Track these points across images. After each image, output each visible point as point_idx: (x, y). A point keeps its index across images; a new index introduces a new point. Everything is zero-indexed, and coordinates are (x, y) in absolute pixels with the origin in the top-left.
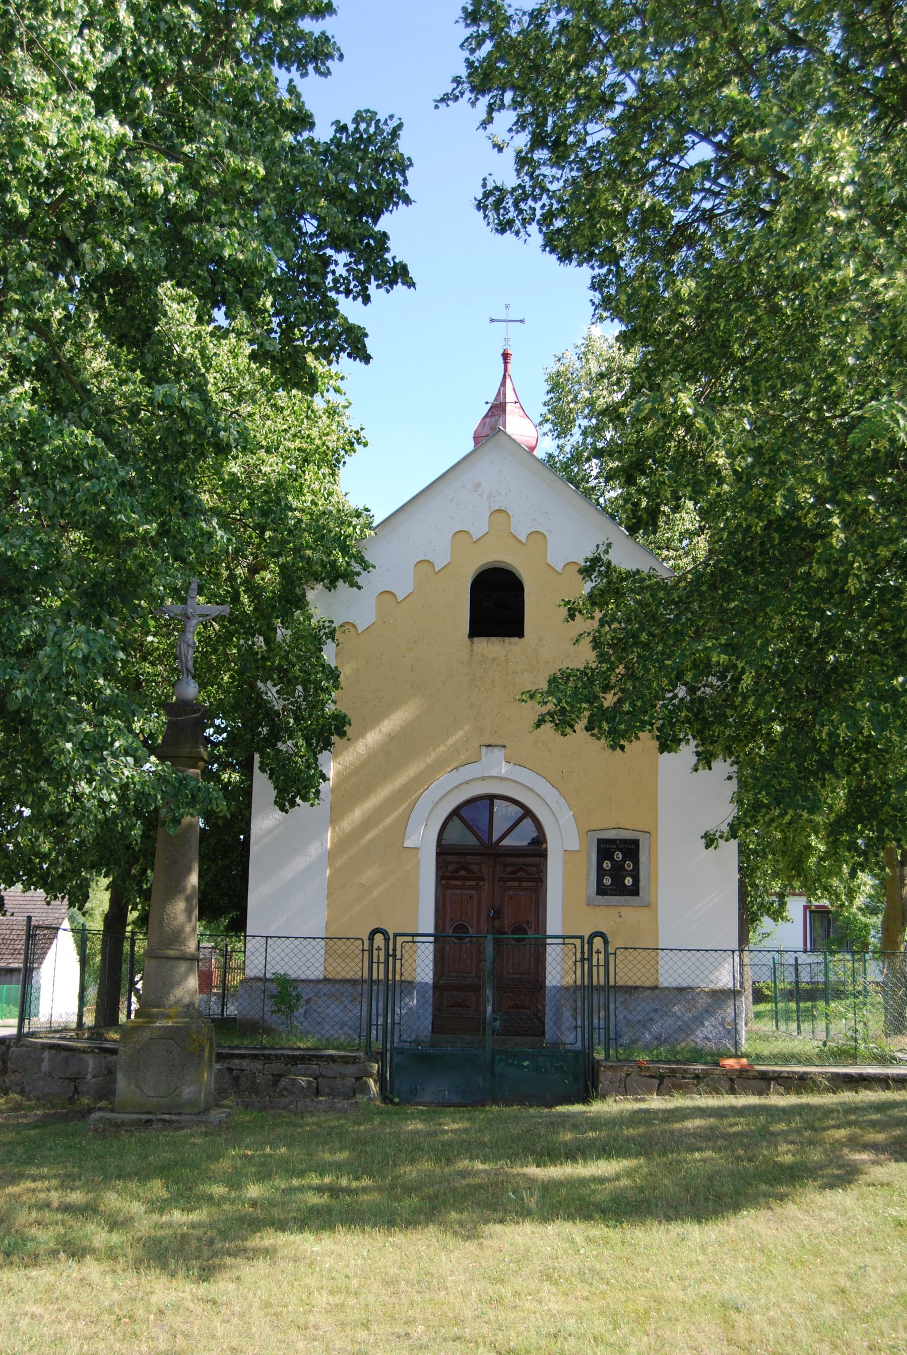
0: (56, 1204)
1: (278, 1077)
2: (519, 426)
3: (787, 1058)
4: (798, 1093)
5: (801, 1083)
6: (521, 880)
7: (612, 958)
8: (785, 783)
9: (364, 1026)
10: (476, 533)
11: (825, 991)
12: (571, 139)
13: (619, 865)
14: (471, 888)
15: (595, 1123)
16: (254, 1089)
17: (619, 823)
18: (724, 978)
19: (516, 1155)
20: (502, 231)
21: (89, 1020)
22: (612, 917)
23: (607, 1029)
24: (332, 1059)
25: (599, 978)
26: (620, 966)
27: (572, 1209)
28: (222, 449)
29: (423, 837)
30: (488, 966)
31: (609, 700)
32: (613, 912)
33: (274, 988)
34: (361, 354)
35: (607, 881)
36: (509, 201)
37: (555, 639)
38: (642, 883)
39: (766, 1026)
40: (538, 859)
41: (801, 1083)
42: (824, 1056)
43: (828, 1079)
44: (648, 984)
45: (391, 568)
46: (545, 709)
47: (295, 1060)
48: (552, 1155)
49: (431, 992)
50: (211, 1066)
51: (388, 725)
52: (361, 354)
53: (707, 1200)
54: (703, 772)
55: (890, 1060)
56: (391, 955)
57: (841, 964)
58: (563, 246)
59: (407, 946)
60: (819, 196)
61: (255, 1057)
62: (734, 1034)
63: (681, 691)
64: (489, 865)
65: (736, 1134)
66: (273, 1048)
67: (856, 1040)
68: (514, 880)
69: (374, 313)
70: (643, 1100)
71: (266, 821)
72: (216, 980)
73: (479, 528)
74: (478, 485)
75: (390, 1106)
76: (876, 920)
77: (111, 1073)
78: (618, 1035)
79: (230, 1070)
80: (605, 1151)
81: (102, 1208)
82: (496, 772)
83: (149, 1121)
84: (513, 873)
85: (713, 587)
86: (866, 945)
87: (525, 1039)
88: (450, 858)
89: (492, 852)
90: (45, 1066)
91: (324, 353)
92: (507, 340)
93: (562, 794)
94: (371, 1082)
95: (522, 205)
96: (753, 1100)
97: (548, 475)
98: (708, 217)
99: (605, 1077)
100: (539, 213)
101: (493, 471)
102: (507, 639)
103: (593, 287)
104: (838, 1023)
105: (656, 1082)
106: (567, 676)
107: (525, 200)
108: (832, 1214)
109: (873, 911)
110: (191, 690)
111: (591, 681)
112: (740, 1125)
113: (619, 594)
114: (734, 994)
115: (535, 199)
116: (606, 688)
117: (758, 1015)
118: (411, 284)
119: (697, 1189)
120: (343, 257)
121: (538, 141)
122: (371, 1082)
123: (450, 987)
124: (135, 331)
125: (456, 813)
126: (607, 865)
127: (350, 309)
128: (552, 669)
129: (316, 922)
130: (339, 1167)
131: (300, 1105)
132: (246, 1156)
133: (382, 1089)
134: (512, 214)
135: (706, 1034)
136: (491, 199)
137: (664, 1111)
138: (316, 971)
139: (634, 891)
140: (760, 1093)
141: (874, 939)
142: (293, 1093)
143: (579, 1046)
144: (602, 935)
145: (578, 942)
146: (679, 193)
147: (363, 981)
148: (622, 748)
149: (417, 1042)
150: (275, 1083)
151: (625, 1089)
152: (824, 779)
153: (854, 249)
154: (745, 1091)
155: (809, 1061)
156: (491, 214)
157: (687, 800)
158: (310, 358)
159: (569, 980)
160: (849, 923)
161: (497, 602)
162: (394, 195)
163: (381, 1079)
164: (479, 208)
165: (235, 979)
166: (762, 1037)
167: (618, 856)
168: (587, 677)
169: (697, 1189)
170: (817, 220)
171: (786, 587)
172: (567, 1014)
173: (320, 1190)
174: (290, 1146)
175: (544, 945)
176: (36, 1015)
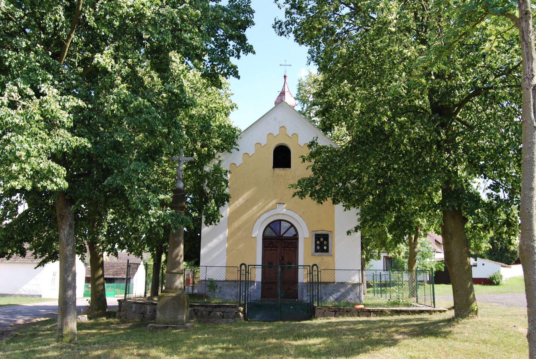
0: (135, 354)
1: (210, 312)
2: (289, 100)
3: (376, 305)
4: (380, 316)
5: (381, 313)
6: (290, 247)
7: (319, 273)
8: (375, 213)
9: (239, 294)
10: (275, 135)
11: (390, 284)
12: (304, 6)
13: (322, 242)
14: (274, 250)
15: (313, 326)
16: (202, 316)
17: (322, 229)
18: (356, 279)
19: (288, 337)
20: (281, 35)
21: (149, 295)
22: (320, 259)
23: (318, 296)
24: (228, 306)
25: (315, 280)
26: (322, 275)
27: (305, 354)
28: (187, 106)
29: (258, 233)
30: (279, 275)
31: (318, 188)
32: (320, 258)
33: (209, 283)
34: (236, 75)
35: (318, 248)
36: (283, 26)
37: (300, 169)
38: (330, 248)
39: (371, 295)
40: (294, 241)
41: (381, 313)
42: (388, 305)
43: (390, 312)
44: (331, 281)
45: (245, 145)
46: (296, 191)
47: (215, 307)
48: (299, 337)
49: (260, 284)
50: (188, 309)
51: (246, 196)
52: (236, 75)
53: (349, 350)
54: (347, 211)
55: (411, 305)
56: (247, 272)
57: (395, 275)
58: (300, 40)
59: (252, 269)
60: (386, 23)
61: (202, 306)
62: (359, 297)
63: (340, 184)
64: (279, 244)
65: (359, 330)
66: (208, 303)
67: (399, 299)
68: (288, 247)
69: (242, 62)
70: (329, 319)
71: (205, 229)
72: (191, 282)
73: (276, 132)
74: (275, 119)
75: (247, 322)
76: (406, 260)
77: (155, 311)
78: (322, 298)
79: (194, 310)
80: (317, 335)
81: (151, 355)
82: (282, 212)
83: (168, 327)
84: (287, 245)
85: (351, 151)
86: (404, 269)
87: (291, 300)
88: (267, 240)
89: (280, 238)
90: (133, 309)
91: (225, 75)
92: (285, 71)
93: (303, 218)
94: (241, 314)
95: (288, 27)
96: (365, 319)
97: (298, 115)
98: (347, 32)
99: (317, 312)
100: (293, 29)
101: (281, 115)
102: (285, 169)
103: (309, 53)
104: (393, 294)
105: (334, 313)
106: (304, 180)
107: (289, 25)
108: (390, 355)
109: (406, 258)
110: (181, 185)
111: (312, 182)
112: (360, 326)
113: (320, 154)
114: (359, 284)
115: (292, 25)
116: (317, 184)
117: (368, 292)
118: (254, 53)
119: (346, 347)
120: (231, 43)
121: (293, 6)
122: (241, 314)
123: (267, 282)
124: (162, 67)
125: (269, 225)
126: (318, 242)
127: (233, 60)
128: (300, 178)
129: (223, 262)
130: (229, 342)
131: (217, 321)
132: (199, 338)
133: (244, 316)
134: (284, 29)
135: (351, 297)
136: (278, 25)
137: (336, 322)
138: (223, 278)
139: (327, 251)
140: (368, 316)
141: (406, 266)
142: (215, 318)
143: (309, 301)
144: (316, 265)
145: (308, 267)
146: (338, 23)
147: (238, 281)
148: (322, 203)
149: (256, 301)
150: (209, 314)
151: (324, 315)
152: (387, 213)
153: (397, 40)
154: (363, 316)
155: (383, 306)
156: (277, 29)
157: (343, 220)
158: (221, 77)
159: (305, 281)
160: (398, 261)
161: (282, 157)
162: (248, 23)
163: (244, 312)
164: (273, 27)
165: (196, 281)
166: (369, 298)
167: (322, 239)
168: (310, 180)
169: (346, 347)
170: (385, 31)
171: (375, 150)
172: (305, 291)
173: (223, 348)
174: (213, 335)
175: (298, 269)
176: (132, 293)
